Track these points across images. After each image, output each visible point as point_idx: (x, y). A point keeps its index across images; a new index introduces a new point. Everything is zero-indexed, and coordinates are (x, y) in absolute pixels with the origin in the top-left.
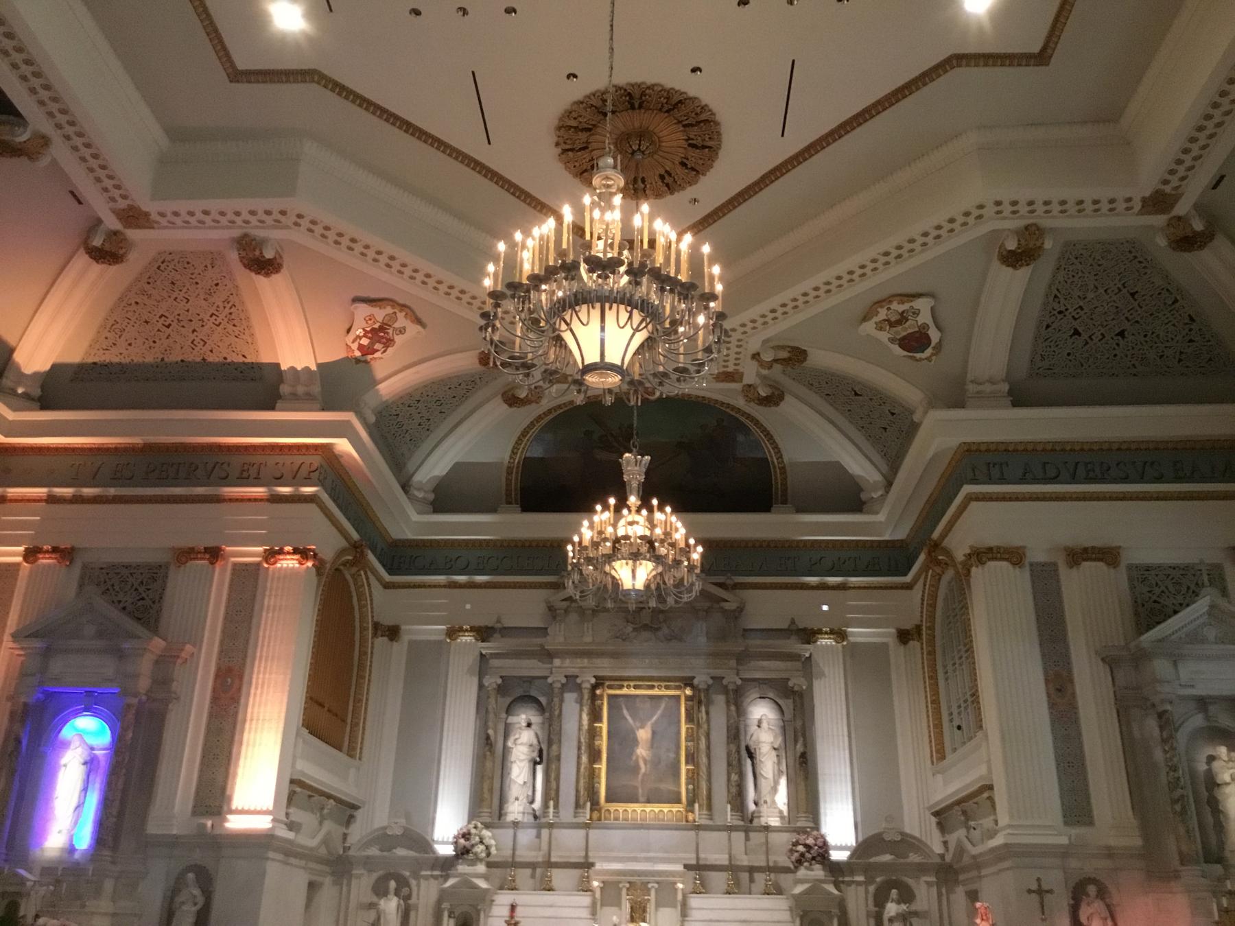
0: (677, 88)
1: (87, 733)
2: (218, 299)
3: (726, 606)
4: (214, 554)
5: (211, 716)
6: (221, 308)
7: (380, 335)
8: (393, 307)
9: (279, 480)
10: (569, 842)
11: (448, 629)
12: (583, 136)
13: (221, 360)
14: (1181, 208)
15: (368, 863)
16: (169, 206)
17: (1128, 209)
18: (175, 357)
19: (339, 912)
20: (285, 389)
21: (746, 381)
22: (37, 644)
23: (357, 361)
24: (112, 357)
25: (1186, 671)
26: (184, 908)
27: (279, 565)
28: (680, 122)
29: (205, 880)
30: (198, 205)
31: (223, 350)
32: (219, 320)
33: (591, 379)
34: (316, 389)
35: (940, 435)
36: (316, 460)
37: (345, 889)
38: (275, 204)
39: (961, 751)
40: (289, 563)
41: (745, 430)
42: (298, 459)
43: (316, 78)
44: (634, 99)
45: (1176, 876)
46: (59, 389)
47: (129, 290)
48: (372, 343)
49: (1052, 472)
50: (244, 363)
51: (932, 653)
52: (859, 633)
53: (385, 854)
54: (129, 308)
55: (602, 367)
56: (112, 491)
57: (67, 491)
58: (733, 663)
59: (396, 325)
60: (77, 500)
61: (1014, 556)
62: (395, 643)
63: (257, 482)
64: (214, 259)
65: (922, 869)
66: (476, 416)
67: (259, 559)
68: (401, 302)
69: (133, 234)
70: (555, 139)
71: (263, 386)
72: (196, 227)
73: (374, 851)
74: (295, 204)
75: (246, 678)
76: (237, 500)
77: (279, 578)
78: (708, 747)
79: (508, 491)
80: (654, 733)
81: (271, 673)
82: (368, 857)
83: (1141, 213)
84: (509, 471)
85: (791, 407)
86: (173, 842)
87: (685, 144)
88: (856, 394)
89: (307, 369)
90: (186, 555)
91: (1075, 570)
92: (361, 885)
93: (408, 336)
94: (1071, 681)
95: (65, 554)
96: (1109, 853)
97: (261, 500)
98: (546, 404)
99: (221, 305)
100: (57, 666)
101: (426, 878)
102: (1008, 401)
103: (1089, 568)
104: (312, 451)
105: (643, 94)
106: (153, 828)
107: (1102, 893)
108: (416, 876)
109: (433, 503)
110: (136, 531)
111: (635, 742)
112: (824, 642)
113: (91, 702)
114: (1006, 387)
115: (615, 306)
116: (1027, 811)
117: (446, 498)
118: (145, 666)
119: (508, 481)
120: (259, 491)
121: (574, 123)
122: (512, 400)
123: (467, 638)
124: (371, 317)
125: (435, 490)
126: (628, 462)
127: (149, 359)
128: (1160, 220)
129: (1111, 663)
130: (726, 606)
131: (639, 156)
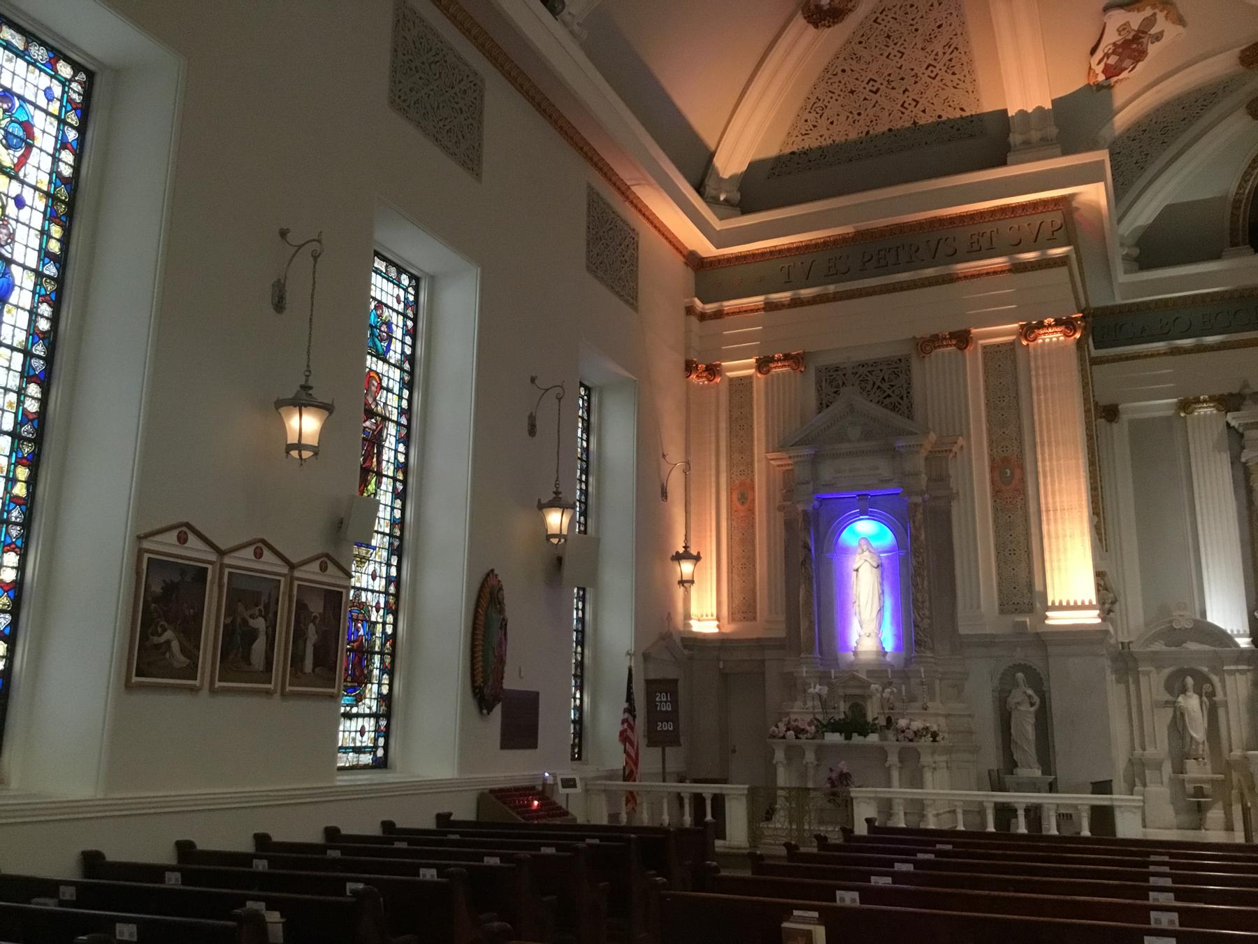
1: (866, 538)
2: (938, 47)
4: (962, 339)
5: (995, 510)
6: (940, 54)
7: (1132, 48)
9: (1019, 246)
11: (1181, 402)
13: (935, 119)
15: (1157, 660)
18: (882, 128)
20: (1015, 138)
22: (806, 451)
23: (1099, 87)
24: (812, 142)
29: (1037, 682)
31: (942, 104)
34: (1053, 131)
37: (1132, 687)
40: (1052, 337)
42: (1036, 220)
46: (764, 187)
50: (962, 118)
53: (1173, 648)
54: (836, 79)
56: (831, 288)
57: (785, 296)
59: (1153, 31)
60: (796, 303)
62: (1114, 425)
63: (991, 252)
66: (1204, 140)
71: (990, 140)
73: (1159, 646)
76: (973, 276)
79: (1233, 231)
82: (1155, 653)
84: (1236, 203)
86: (988, 642)
89: (1040, 109)
92: (1153, 683)
95: (796, 360)
97: (1003, 272)
99: (940, 54)
100: (827, 472)
101: (1232, 673)
108: (1221, 673)
109: (1137, 259)
110: (869, 325)
112: (1202, 411)
113: (868, 506)
117: (1153, 250)
118: (919, 462)
120: (998, 262)
123: (1206, 410)
124: (1125, 27)
125: (1138, 244)
127: (853, 136)
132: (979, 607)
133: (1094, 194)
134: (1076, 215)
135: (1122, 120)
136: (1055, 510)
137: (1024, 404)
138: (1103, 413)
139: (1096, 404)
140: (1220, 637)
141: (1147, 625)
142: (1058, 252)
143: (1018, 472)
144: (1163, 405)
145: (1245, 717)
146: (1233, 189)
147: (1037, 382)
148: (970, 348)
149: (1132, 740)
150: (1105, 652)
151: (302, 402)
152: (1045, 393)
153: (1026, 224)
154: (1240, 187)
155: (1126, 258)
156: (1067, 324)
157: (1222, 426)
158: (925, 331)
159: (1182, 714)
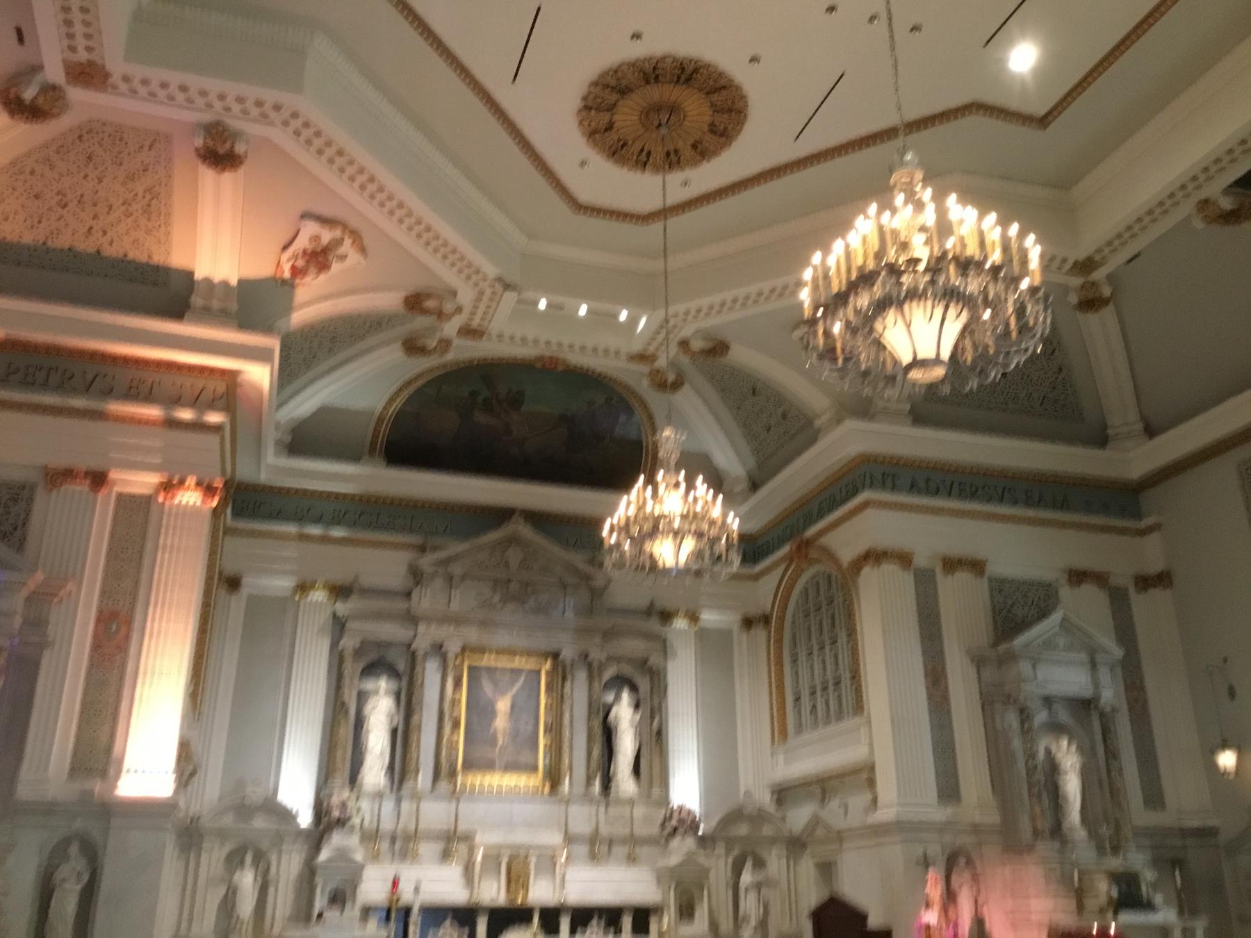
2: (139, 188)
4: (98, 479)
6: (140, 194)
7: (319, 258)
9: (177, 401)
10: (435, 813)
12: (615, 97)
14: (1099, 275)
15: (222, 835)
16: (138, 71)
18: (63, 242)
19: (184, 890)
20: (197, 300)
23: (284, 282)
25: (1043, 672)
26: (67, 886)
29: (93, 855)
30: (175, 78)
32: (57, 198)
33: (915, 375)
34: (234, 306)
38: (270, 96)
39: (806, 736)
40: (190, 497)
41: (629, 410)
44: (652, 72)
45: (1030, 848)
47: (28, 154)
51: (779, 641)
52: (710, 617)
55: (916, 363)
58: (598, 640)
61: (904, 559)
62: (234, 598)
63: (148, 397)
65: (773, 841)
69: (76, 94)
71: (172, 294)
72: (144, 99)
73: (228, 820)
74: (290, 100)
75: (136, 625)
77: (177, 515)
78: (571, 722)
80: (513, 706)
81: (168, 621)
84: (380, 420)
85: (686, 399)
86: (49, 809)
87: (706, 128)
89: (225, 284)
90: (58, 477)
92: (213, 858)
93: (348, 264)
94: (946, 677)
96: (976, 829)
98: (450, 356)
99: (140, 194)
103: (963, 576)
105: (696, 71)
106: (25, 790)
107: (969, 862)
111: (493, 714)
114: (908, 407)
116: (901, 787)
117: (304, 440)
118: (17, 602)
120: (153, 412)
122: (413, 347)
124: (316, 238)
126: (668, 438)
127: (27, 239)
129: (979, 662)
131: (663, 131)
132: (46, 769)
133: (259, 375)
134: (239, 390)
135: (299, 317)
136: (153, 674)
137: (146, 561)
138: (223, 581)
139: (220, 573)
140: (286, 816)
141: (220, 798)
142: (214, 418)
143: (124, 629)
144: (282, 584)
145: (291, 895)
146: (379, 408)
147: (165, 540)
148: (104, 491)
149: (181, 914)
150: (169, 826)
151: (1225, 745)
152: (171, 553)
153: (190, 384)
154: (385, 408)
155: (278, 443)
156: (209, 490)
157: (329, 612)
158: (59, 461)
159: (234, 893)
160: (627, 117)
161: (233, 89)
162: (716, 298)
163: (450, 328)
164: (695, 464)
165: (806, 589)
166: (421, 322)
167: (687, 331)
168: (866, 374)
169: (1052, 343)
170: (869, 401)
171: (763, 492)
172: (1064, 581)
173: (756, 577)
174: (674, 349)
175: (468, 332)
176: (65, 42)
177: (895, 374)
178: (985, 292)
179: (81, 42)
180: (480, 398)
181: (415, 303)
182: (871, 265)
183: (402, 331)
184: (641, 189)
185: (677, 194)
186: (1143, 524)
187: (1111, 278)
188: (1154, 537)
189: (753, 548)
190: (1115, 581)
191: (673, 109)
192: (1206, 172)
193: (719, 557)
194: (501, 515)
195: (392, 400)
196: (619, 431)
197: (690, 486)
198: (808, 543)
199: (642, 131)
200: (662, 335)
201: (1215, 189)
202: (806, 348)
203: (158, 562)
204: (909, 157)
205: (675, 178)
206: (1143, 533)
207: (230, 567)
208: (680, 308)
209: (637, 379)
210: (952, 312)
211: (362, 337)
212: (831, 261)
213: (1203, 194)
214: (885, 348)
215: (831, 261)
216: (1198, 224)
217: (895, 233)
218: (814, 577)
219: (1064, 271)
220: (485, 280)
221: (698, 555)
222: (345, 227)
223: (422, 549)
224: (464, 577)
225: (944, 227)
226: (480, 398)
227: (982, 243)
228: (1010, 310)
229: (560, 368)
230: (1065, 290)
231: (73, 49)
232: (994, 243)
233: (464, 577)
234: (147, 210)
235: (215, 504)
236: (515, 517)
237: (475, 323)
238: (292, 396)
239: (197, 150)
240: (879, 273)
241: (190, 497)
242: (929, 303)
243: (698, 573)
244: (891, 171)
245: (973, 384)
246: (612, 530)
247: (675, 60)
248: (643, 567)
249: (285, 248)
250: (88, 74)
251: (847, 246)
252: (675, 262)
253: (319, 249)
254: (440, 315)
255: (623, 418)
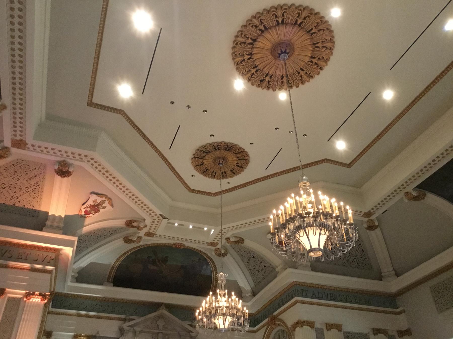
0: (243, 147)
3: (192, 334)
7: (96, 208)
8: (106, 198)
9: (36, 261)
12: (204, 154)
13: (22, 206)
14: (373, 217)
16: (37, 143)
17: (359, 214)
20: (48, 223)
21: (218, 247)
23: (82, 216)
27: (31, 300)
28: (237, 158)
31: (25, 201)
32: (29, 190)
34: (62, 225)
35: (287, 278)
36: (53, 255)
38: (84, 152)
40: (36, 300)
41: (208, 264)
42: (45, 254)
43: (122, 113)
44: (217, 147)
48: (91, 210)
49: (321, 296)
50: (32, 209)
55: (312, 250)
59: (103, 205)
61: (311, 325)
64: (41, 167)
67: (21, 296)
68: (109, 196)
70: (194, 152)
71: (39, 221)
72: (32, 151)
74: (90, 154)
79: (109, 276)
83: (362, 217)
84: (113, 268)
85: (228, 259)
87: (235, 165)
88: (253, 257)
89: (60, 217)
91: (329, 331)
97: (27, 269)
98: (141, 243)
102: (310, 269)
103: (334, 331)
104: (53, 251)
109: (76, 278)
114: (310, 264)
115: (312, 228)
117: (82, 276)
119: (111, 272)
120: (27, 265)
121: (204, 150)
122: (127, 240)
124: (95, 201)
125: (79, 273)
126: (221, 276)
128: (366, 219)
130: (192, 334)
131: (221, 165)
133: (68, 251)
134: (60, 256)
135: (86, 229)
137: (16, 325)
139: (45, 330)
146: (113, 263)
153: (42, 254)
155: (73, 276)
156: (43, 296)
160: (208, 161)
161: (70, 149)
162: (239, 223)
163: (142, 233)
164: (233, 287)
165: (275, 336)
166: (131, 230)
167: (228, 235)
168: (294, 253)
169: (359, 243)
170: (295, 262)
171: (257, 296)
172: (371, 333)
173: (255, 332)
174: (224, 241)
175: (149, 234)
176: (13, 133)
177: (304, 254)
178: (334, 225)
179: (18, 133)
180: (151, 259)
181: (129, 224)
182: (294, 214)
183: (124, 234)
184: (213, 185)
185: (225, 187)
186: (398, 310)
187: (377, 218)
188: (403, 316)
189: (254, 320)
190: (390, 333)
191: (224, 159)
192: (406, 183)
193: (241, 324)
194: (156, 306)
195: (117, 261)
196: (203, 272)
197: (230, 296)
198: (275, 318)
199: (213, 165)
200: (219, 236)
201: (410, 189)
202: (272, 243)
203: (20, 326)
204: (304, 177)
205: (225, 181)
206: (399, 313)
207: (48, 329)
208: (226, 226)
209: (210, 252)
210: (323, 232)
211: (109, 236)
212: (280, 212)
213: (406, 190)
214: (300, 243)
215: (280, 212)
216: (406, 200)
217: (301, 203)
218: (277, 332)
219: (361, 215)
220: (156, 215)
221: (233, 323)
222: (106, 196)
223: (124, 320)
224: (141, 332)
225: (318, 202)
226: (151, 259)
227: (331, 206)
228: (344, 231)
229: (182, 248)
230: (362, 222)
231: (15, 135)
232: (336, 207)
233: (141, 332)
234: (34, 191)
235: (46, 301)
236: (163, 306)
237: (151, 231)
238: (78, 260)
239: (55, 170)
240: (297, 217)
241: (36, 300)
242: (315, 228)
243: (233, 330)
244: (299, 182)
245: (332, 257)
246: (199, 314)
247: (225, 143)
248: (212, 328)
249: (83, 204)
250: (19, 144)
251: (285, 207)
252: (225, 209)
253: (96, 204)
254: (139, 228)
255: (205, 267)
